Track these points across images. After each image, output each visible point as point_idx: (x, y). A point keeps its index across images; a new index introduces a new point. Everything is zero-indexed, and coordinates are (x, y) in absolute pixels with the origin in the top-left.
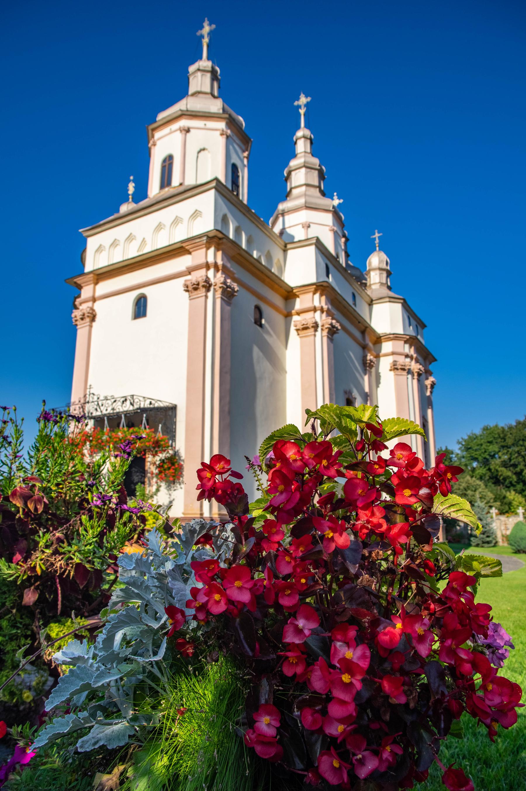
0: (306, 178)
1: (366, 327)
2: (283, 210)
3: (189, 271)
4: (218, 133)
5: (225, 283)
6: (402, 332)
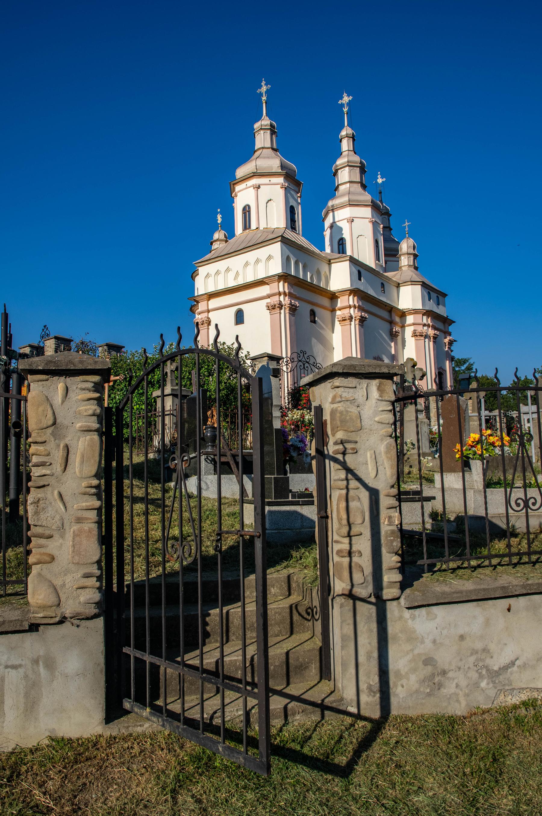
0: (350, 176)
1: (392, 308)
2: (333, 206)
3: (269, 296)
4: (279, 186)
5: (291, 304)
6: (421, 308)
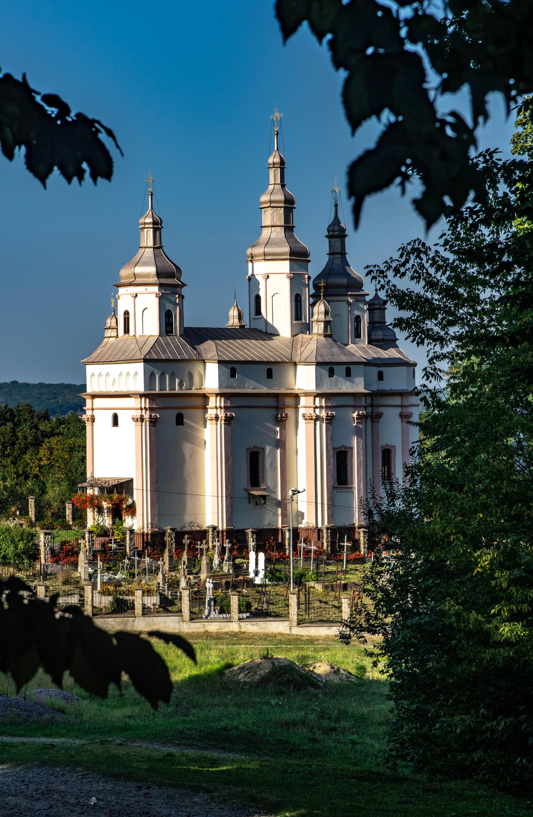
4: (154, 295)
